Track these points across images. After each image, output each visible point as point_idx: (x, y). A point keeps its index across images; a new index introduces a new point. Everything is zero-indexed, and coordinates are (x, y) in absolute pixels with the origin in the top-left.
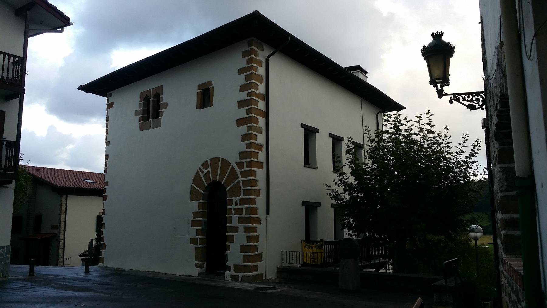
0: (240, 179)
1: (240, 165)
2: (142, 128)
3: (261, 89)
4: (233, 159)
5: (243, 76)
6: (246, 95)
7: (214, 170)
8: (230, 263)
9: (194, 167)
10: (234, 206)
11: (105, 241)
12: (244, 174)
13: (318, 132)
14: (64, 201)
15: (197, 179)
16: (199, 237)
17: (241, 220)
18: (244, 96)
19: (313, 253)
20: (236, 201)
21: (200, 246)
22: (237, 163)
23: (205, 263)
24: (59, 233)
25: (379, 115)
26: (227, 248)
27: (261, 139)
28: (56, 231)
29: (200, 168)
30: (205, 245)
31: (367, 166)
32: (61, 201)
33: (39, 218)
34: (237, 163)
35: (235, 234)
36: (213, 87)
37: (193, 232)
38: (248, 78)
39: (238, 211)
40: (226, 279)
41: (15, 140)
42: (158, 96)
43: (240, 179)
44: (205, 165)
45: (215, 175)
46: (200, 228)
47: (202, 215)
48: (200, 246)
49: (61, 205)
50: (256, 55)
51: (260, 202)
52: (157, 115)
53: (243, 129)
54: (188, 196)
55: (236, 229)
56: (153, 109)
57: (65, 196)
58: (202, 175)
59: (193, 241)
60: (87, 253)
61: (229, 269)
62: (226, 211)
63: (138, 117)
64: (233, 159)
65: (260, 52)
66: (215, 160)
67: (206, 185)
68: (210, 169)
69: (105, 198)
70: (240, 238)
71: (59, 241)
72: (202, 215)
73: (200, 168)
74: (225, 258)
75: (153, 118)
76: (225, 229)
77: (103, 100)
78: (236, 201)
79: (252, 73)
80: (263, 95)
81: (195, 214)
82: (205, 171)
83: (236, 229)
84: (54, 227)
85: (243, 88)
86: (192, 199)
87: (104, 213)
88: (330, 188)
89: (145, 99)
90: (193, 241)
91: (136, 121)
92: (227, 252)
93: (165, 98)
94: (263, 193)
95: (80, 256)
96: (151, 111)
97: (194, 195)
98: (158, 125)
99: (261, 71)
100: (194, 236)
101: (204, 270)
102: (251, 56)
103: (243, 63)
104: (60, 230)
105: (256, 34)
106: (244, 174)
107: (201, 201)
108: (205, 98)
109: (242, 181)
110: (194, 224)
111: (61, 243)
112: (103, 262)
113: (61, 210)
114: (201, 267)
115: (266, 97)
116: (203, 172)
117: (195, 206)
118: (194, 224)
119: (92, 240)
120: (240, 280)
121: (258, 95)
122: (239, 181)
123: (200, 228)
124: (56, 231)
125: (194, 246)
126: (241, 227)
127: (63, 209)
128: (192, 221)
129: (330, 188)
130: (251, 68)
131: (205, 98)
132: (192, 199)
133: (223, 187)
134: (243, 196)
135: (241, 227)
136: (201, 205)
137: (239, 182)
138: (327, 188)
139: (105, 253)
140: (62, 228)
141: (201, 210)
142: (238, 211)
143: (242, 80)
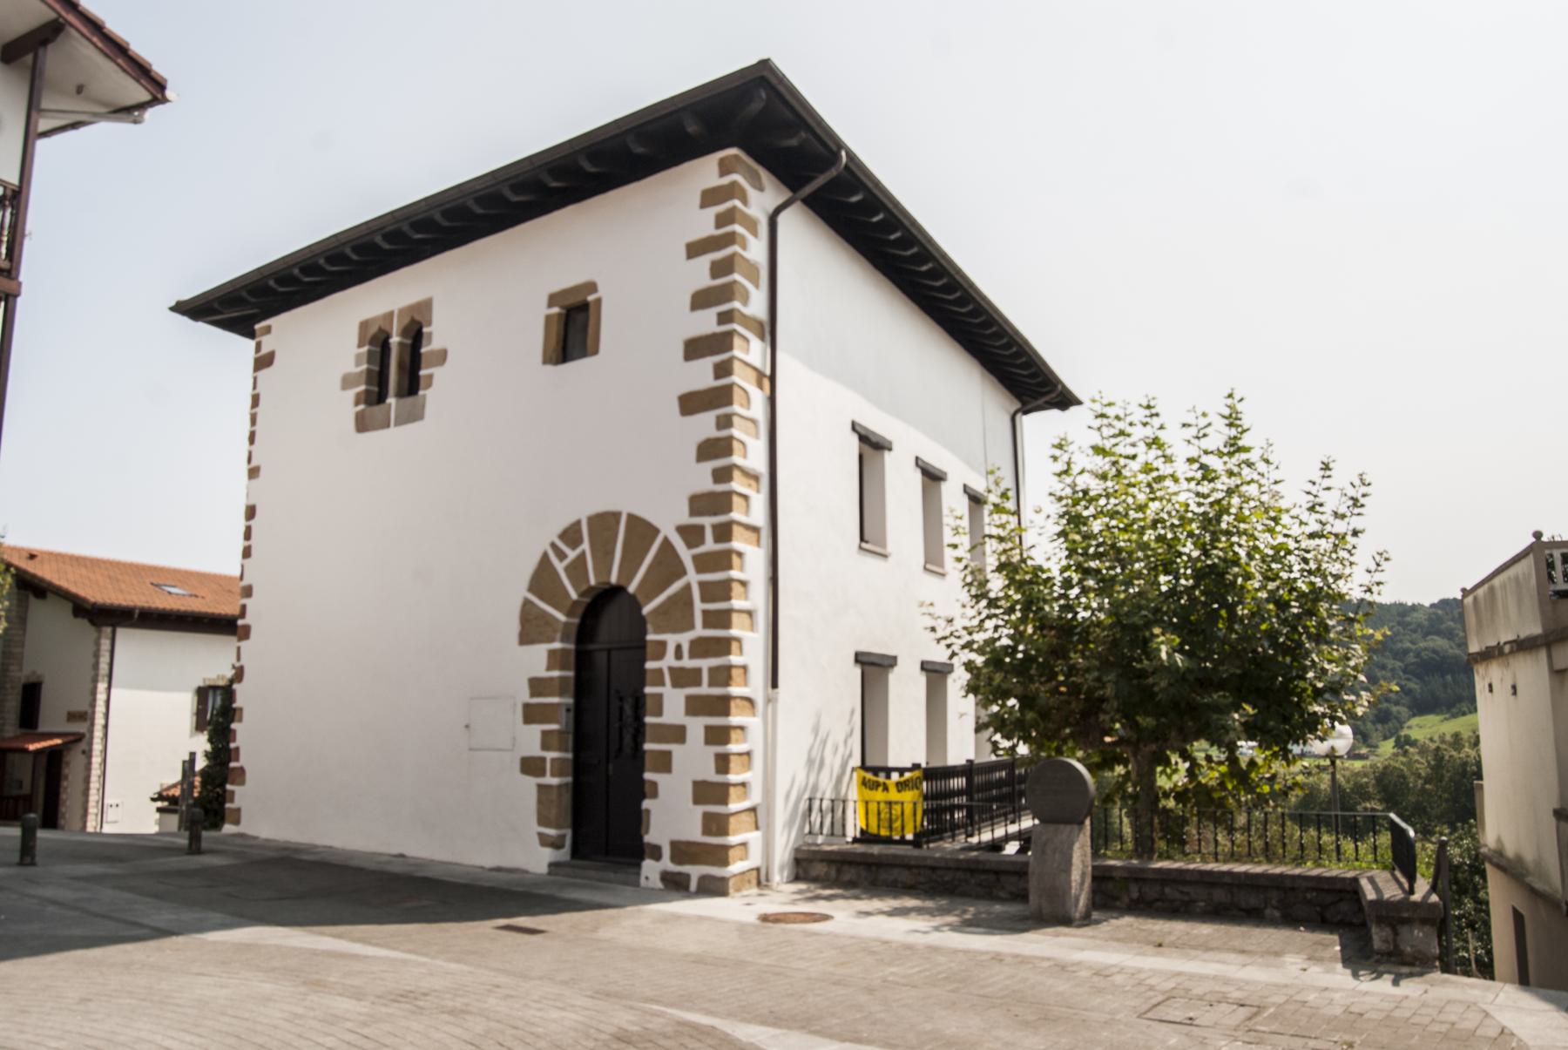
0: (693, 577)
1: (692, 535)
2: (362, 425)
3: (756, 306)
4: (668, 517)
5: (705, 261)
6: (714, 319)
7: (603, 551)
8: (659, 832)
9: (539, 538)
10: (669, 660)
11: (244, 761)
12: (703, 563)
13: (890, 449)
14: (105, 644)
15: (543, 581)
16: (551, 755)
17: (696, 706)
18: (706, 323)
19: (890, 804)
20: (679, 648)
21: (555, 781)
22: (683, 530)
23: (568, 833)
24: (91, 731)
25: (1019, 416)
26: (642, 790)
27: (752, 455)
28: (79, 727)
29: (553, 545)
30: (569, 779)
31: (1242, 526)
32: (98, 644)
33: (31, 694)
34: (683, 530)
35: (674, 748)
36: (599, 301)
37: (530, 739)
38: (719, 269)
39: (684, 678)
40: (643, 881)
41: (14, 179)
42: (416, 334)
43: (693, 577)
44: (571, 535)
45: (629, 566)
46: (554, 727)
47: (560, 687)
48: (555, 781)
49: (97, 655)
50: (745, 201)
51: (750, 650)
52: (412, 385)
53: (704, 425)
54: (514, 627)
55: (679, 734)
56: (401, 366)
57: (109, 630)
58: (560, 567)
59: (531, 766)
60: (177, 792)
61: (656, 853)
62: (641, 677)
63: (351, 394)
64: (668, 517)
65: (752, 193)
66: (604, 523)
67: (574, 595)
68: (586, 546)
69: (244, 633)
70: (692, 759)
71: (88, 754)
72: (560, 687)
73: (553, 545)
74: (638, 820)
75: (400, 395)
76: (639, 732)
77: (241, 348)
78: (679, 648)
79: (734, 255)
80: (761, 324)
81: (537, 686)
82: (572, 555)
83: (679, 734)
84: (74, 717)
85: (701, 300)
86: (526, 638)
87: (239, 674)
88: (931, 610)
89: (377, 341)
90: (531, 766)
91: (346, 405)
92: (647, 804)
93: (438, 335)
94: (762, 619)
95: (153, 800)
96: (395, 371)
97: (531, 628)
98: (416, 415)
99: (756, 250)
100: (535, 750)
101: (564, 854)
102: (728, 205)
103: (704, 224)
104: (92, 724)
105: (757, 124)
106: (703, 563)
107: (557, 645)
108: (573, 329)
109: (702, 585)
110: (531, 714)
111: (96, 760)
112: (237, 822)
113: (96, 666)
114: (556, 844)
115: (769, 330)
116: (562, 556)
117: (536, 660)
118: (531, 714)
119: (193, 755)
120: (693, 886)
121: (748, 322)
122: (687, 588)
123: (554, 727)
124: (79, 727)
125: (531, 782)
126: (696, 727)
127: (104, 667)
128: (526, 706)
129: (931, 610)
130: (730, 239)
131: (573, 329)
132: (526, 638)
133: (635, 604)
134: (699, 631)
135: (696, 727)
136: (555, 659)
137: (688, 587)
138: (924, 610)
139: (241, 796)
140: (99, 720)
141: (556, 673)
142: (684, 678)
143: (699, 274)
